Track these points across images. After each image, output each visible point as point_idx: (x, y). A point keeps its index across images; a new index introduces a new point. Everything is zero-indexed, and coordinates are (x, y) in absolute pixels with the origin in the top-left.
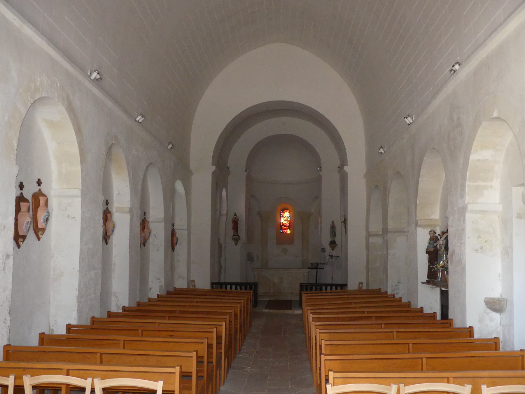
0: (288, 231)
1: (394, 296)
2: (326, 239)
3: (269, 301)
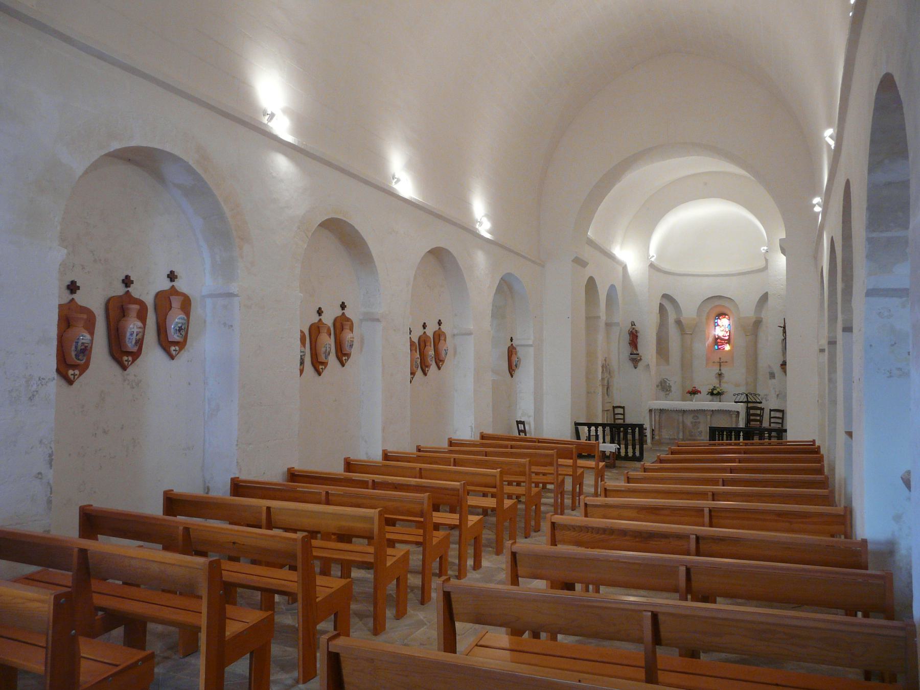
0: (727, 347)
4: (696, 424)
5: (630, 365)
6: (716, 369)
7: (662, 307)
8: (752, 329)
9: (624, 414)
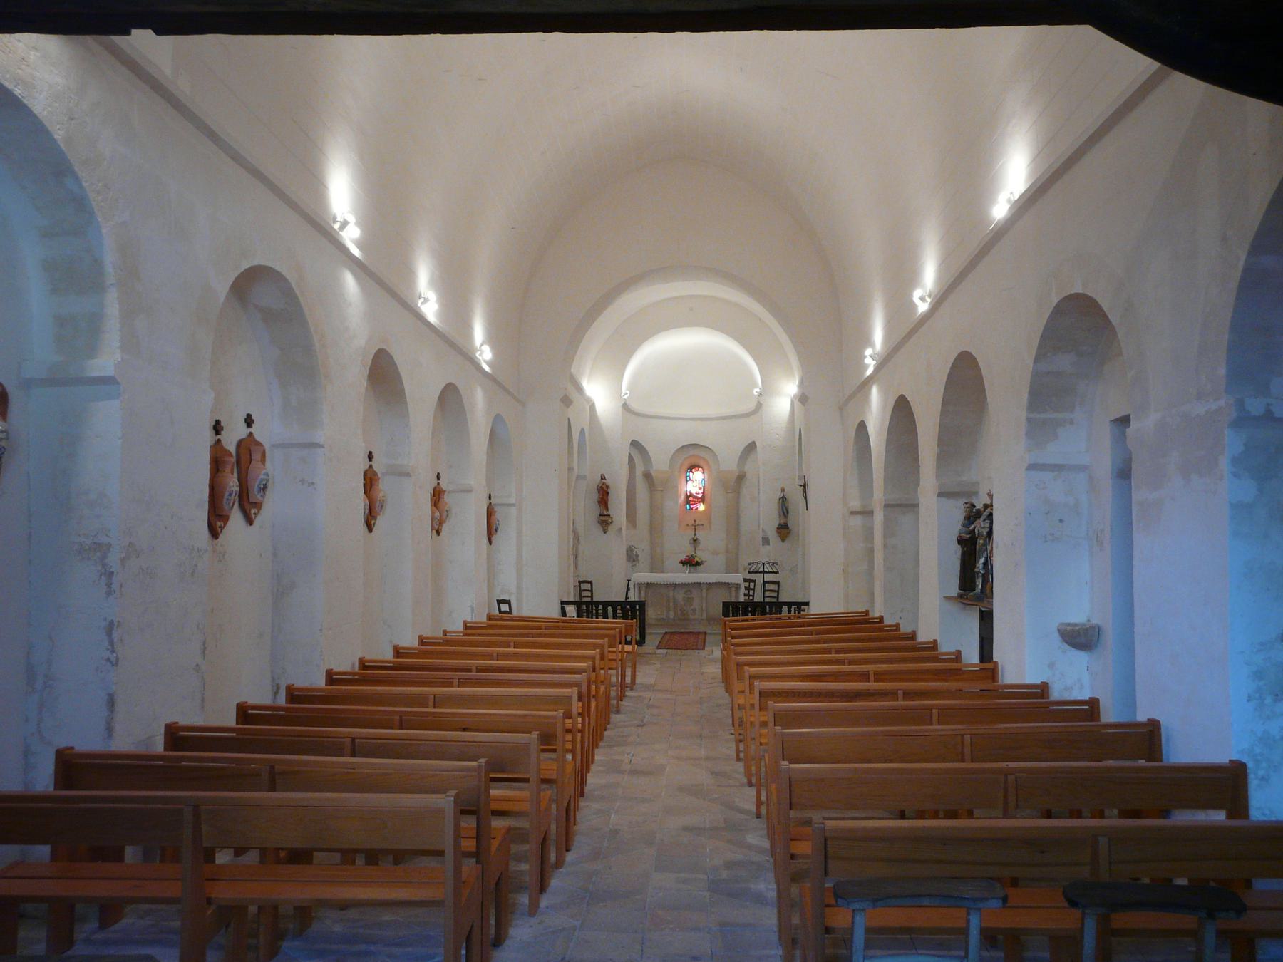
0: (701, 507)
1: (897, 627)
2: (770, 520)
3: (510, 829)
4: (689, 600)
5: (597, 530)
6: (690, 534)
7: (631, 459)
9: (591, 591)
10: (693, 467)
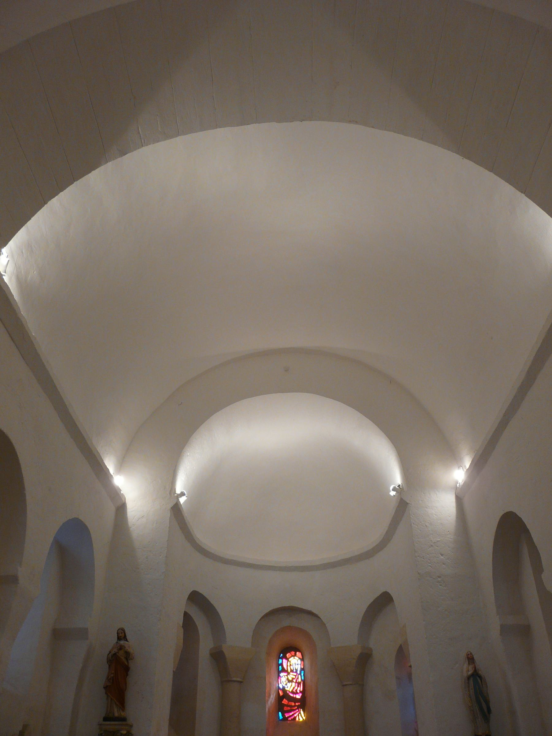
0: (301, 716)
7: (188, 622)
8: (349, 672)
10: (287, 650)
